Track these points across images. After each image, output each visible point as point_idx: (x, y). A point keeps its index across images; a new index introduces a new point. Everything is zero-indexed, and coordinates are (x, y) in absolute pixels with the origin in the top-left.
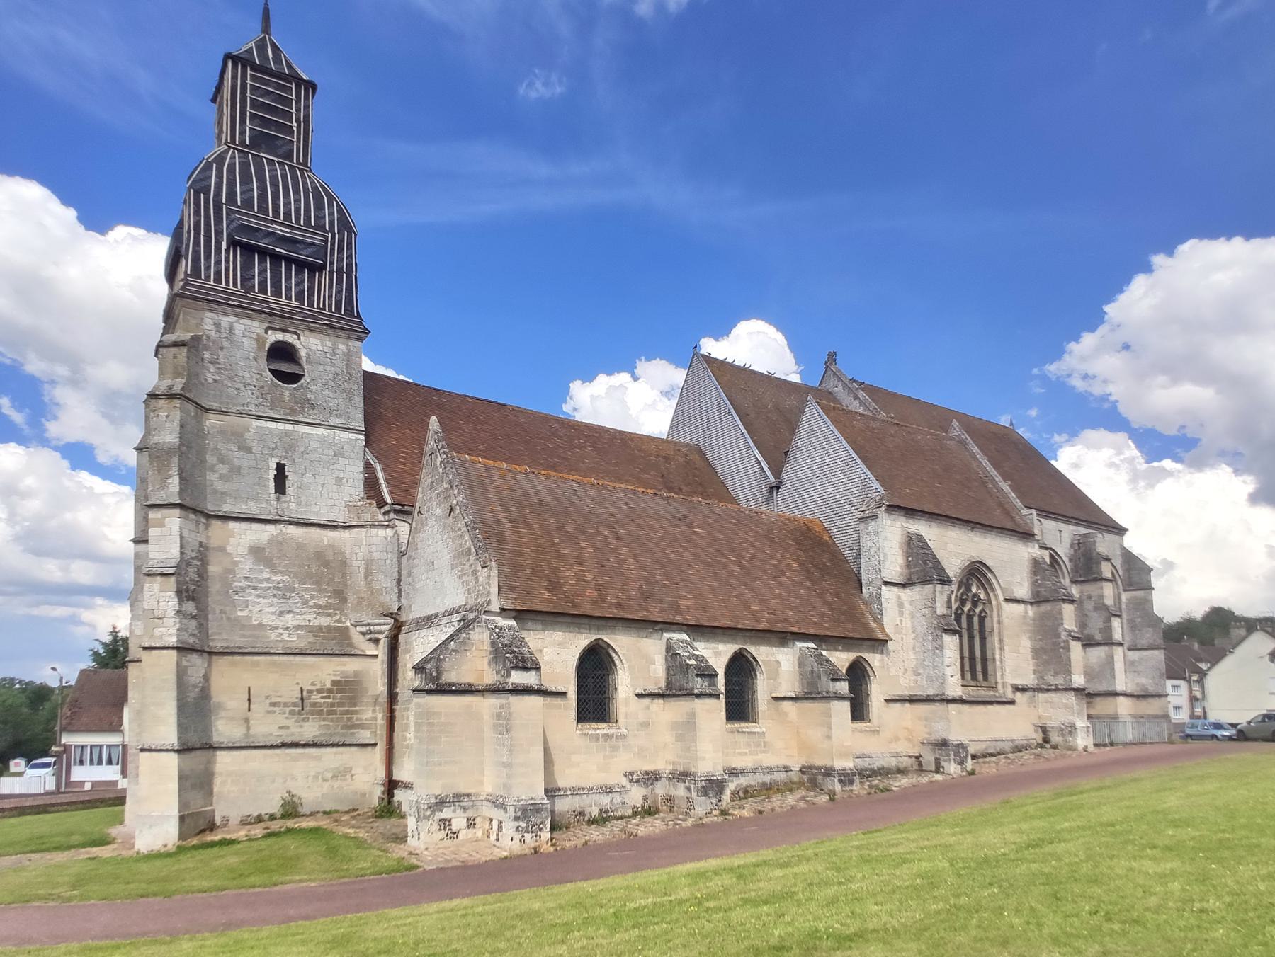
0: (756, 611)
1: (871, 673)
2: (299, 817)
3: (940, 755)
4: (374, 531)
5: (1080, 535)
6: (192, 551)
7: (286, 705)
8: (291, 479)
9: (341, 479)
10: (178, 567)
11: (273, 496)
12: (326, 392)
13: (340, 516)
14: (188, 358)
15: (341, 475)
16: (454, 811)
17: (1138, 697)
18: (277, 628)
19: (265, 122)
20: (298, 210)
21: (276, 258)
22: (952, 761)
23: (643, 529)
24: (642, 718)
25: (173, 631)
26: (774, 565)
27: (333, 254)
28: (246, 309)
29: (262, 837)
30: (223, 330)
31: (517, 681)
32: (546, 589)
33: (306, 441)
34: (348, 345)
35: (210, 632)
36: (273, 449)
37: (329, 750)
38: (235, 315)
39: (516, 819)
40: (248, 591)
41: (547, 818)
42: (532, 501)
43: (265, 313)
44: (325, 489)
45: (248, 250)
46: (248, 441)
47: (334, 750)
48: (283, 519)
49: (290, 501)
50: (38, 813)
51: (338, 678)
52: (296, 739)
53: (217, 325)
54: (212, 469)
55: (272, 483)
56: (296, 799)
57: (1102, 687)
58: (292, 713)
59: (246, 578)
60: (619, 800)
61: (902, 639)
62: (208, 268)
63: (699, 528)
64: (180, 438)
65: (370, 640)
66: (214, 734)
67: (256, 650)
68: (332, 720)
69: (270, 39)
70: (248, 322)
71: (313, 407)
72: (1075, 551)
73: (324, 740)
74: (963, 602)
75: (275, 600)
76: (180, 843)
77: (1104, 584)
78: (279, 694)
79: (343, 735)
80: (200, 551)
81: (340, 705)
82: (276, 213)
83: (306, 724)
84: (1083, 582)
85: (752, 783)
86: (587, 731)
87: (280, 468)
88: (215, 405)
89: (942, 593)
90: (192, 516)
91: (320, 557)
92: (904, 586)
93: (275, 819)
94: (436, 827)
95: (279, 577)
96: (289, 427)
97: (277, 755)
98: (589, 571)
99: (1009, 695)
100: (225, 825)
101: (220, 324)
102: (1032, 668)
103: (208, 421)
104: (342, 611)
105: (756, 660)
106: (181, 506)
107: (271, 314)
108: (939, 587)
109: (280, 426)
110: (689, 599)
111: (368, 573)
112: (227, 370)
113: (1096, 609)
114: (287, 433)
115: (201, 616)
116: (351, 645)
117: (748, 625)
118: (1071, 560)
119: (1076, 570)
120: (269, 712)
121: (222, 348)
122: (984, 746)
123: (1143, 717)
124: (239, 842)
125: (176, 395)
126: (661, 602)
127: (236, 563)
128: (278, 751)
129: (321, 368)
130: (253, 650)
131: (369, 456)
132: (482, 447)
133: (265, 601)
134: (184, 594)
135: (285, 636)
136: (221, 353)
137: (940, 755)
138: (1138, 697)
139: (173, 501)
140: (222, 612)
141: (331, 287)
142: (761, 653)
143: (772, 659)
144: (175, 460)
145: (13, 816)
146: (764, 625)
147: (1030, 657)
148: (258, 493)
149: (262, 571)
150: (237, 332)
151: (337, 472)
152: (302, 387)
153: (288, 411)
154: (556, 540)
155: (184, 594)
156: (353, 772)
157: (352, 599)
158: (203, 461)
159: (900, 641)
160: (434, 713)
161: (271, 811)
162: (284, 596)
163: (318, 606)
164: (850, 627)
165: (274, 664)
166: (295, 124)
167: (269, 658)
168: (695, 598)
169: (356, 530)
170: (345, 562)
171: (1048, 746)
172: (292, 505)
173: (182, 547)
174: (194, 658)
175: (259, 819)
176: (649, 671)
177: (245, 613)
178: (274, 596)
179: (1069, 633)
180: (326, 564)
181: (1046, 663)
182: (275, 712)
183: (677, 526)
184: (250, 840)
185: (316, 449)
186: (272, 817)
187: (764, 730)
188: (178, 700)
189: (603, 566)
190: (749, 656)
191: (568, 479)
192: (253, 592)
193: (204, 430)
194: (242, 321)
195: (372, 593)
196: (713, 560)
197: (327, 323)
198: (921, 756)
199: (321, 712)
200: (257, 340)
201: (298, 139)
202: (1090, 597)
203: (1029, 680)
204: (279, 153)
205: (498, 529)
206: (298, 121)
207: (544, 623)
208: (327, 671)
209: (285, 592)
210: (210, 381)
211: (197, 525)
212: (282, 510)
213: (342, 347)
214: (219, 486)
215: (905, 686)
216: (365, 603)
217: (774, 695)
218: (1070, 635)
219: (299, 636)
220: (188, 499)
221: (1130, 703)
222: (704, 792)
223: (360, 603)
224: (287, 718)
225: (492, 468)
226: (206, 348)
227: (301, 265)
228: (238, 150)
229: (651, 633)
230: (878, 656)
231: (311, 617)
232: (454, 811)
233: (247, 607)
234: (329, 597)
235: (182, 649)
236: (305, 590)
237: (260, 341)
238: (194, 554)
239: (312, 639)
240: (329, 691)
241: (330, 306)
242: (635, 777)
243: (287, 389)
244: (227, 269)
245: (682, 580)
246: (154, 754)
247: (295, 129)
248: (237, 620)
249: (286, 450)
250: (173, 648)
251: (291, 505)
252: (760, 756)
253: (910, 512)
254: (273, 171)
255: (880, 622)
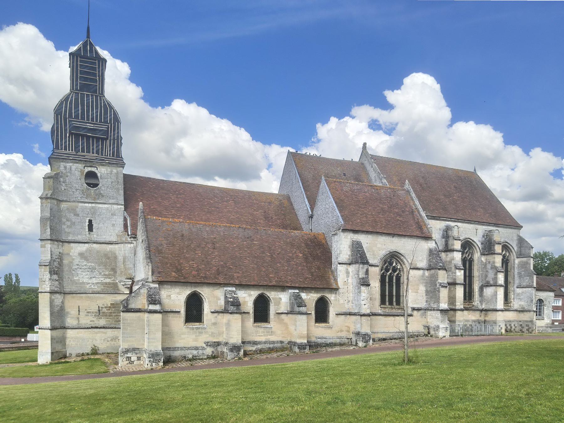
0: (272, 277)
1: (330, 303)
2: (97, 354)
3: (357, 338)
4: (126, 245)
5: (488, 231)
6: (56, 256)
7: (93, 312)
8: (95, 225)
9: (114, 224)
10: (50, 262)
11: (87, 233)
12: (108, 190)
13: (114, 239)
14: (53, 182)
15: (114, 223)
16: (132, 354)
17: (520, 311)
18: (89, 284)
19: (86, 79)
20: (97, 116)
21: (88, 137)
22: (361, 341)
23: (228, 244)
24: (213, 321)
25: (48, 286)
26: (289, 256)
27: (111, 133)
28: (75, 161)
29: (79, 361)
30: (67, 169)
31: (151, 308)
32: (174, 272)
33: (100, 210)
34: (117, 170)
35: (64, 285)
36: (87, 214)
37: (109, 330)
38: (72, 162)
39: (149, 358)
40: (78, 270)
41: (162, 358)
42: (179, 235)
43: (83, 161)
44: (108, 229)
45: (77, 136)
46: (78, 212)
47: (111, 330)
48: (91, 241)
49: (94, 234)
50: (25, 349)
51: (113, 303)
52: (97, 325)
53: (65, 167)
54: (64, 224)
55: (87, 228)
56: (97, 348)
57: (492, 307)
58: (95, 316)
59: (78, 265)
60: (201, 352)
61: (348, 287)
62: (62, 145)
63: (256, 241)
64: (50, 214)
65: (126, 287)
66: (66, 323)
67: (81, 292)
68: (111, 319)
69: (89, 40)
70: (77, 165)
71: (103, 196)
72: (485, 239)
73: (107, 326)
74: (387, 270)
75: (89, 273)
76: (51, 362)
77: (496, 256)
78: (90, 308)
79: (115, 324)
80: (59, 256)
81: (114, 313)
82: (88, 119)
83: (101, 320)
84: (487, 254)
85: (264, 347)
86: (188, 326)
87: (90, 221)
88: (65, 199)
89: (363, 268)
90: (56, 243)
91: (106, 256)
92: (350, 264)
93: (89, 355)
94: (125, 359)
95: (90, 264)
96: (93, 205)
97: (90, 331)
98: (196, 263)
99: (415, 313)
100: (70, 356)
101: (66, 167)
102: (425, 299)
103: (62, 205)
104: (115, 276)
105: (269, 298)
106: (51, 240)
107: (85, 161)
108: (361, 266)
109: (90, 205)
110: (240, 273)
111: (124, 262)
112: (69, 184)
113: (492, 268)
114: (93, 207)
115: (60, 280)
116: (118, 290)
117: (265, 283)
118: (482, 244)
119: (484, 249)
120: (86, 315)
121: (67, 176)
122: (391, 335)
123: (521, 322)
124: (71, 362)
125: (48, 198)
126: (226, 275)
127: (73, 259)
128: (90, 330)
129: (106, 180)
130: (80, 292)
131: (126, 214)
132: (178, 205)
133: (85, 273)
134: (53, 272)
135: (92, 287)
136: (67, 178)
137: (357, 338)
138: (520, 311)
139: (48, 238)
140: (68, 278)
141: (110, 146)
142: (272, 295)
143: (277, 297)
144: (49, 222)
145: (16, 350)
146: (274, 283)
147: (424, 295)
148: (82, 232)
149: (83, 262)
150: (73, 169)
151: (113, 222)
152: (98, 189)
153: (93, 199)
154: (185, 251)
155: (53, 272)
156: (119, 338)
157: (118, 272)
158: (60, 221)
159: (346, 288)
160: (125, 319)
161: (87, 352)
162: (92, 271)
163: (105, 275)
164: (319, 283)
165: (88, 297)
166: (98, 78)
167: (86, 295)
168: (243, 273)
169: (120, 245)
170: (116, 257)
171: (429, 335)
172: (95, 236)
173: (51, 255)
174: (57, 295)
175: (83, 355)
176: (217, 303)
177: (77, 278)
178: (88, 271)
179: (440, 284)
180: (109, 258)
181: (431, 297)
182: (89, 315)
183: (246, 241)
184: (75, 362)
185: (104, 213)
186: (88, 354)
187: (272, 326)
188: (50, 311)
189: (203, 261)
190: (266, 296)
191: (199, 224)
192: (80, 270)
193: (61, 209)
194: (75, 165)
195: (126, 269)
196: (258, 256)
197: (108, 162)
198: (352, 339)
199: (106, 315)
200: (81, 172)
201: (99, 84)
202: (489, 262)
203: (423, 305)
204: (91, 91)
205: (160, 248)
206: (99, 76)
207: (171, 285)
208: (109, 300)
209: (92, 270)
210: (63, 189)
211: (58, 246)
212: (91, 238)
213: (115, 171)
214: (67, 230)
215: (348, 307)
216: (123, 273)
217: (277, 312)
218: (440, 285)
219: (98, 287)
220: (54, 237)
221: (515, 314)
222: (231, 350)
223: (121, 273)
224: (93, 318)
225: (164, 222)
226: (61, 177)
227: (98, 139)
228: (75, 92)
229: (219, 288)
230: (333, 295)
231: (102, 279)
232: (132, 354)
233: (78, 276)
234: (110, 271)
235: (52, 293)
236: (100, 269)
237: (82, 172)
238: (56, 257)
239: (103, 288)
240: (110, 307)
241: (110, 154)
242: (209, 344)
243: (92, 190)
244: (69, 144)
245: (239, 265)
246: (43, 330)
247: (98, 80)
248: (74, 281)
249: (92, 214)
250: (48, 292)
251: (94, 236)
252: (269, 337)
253: (355, 232)
254: (88, 100)
255: (336, 280)
